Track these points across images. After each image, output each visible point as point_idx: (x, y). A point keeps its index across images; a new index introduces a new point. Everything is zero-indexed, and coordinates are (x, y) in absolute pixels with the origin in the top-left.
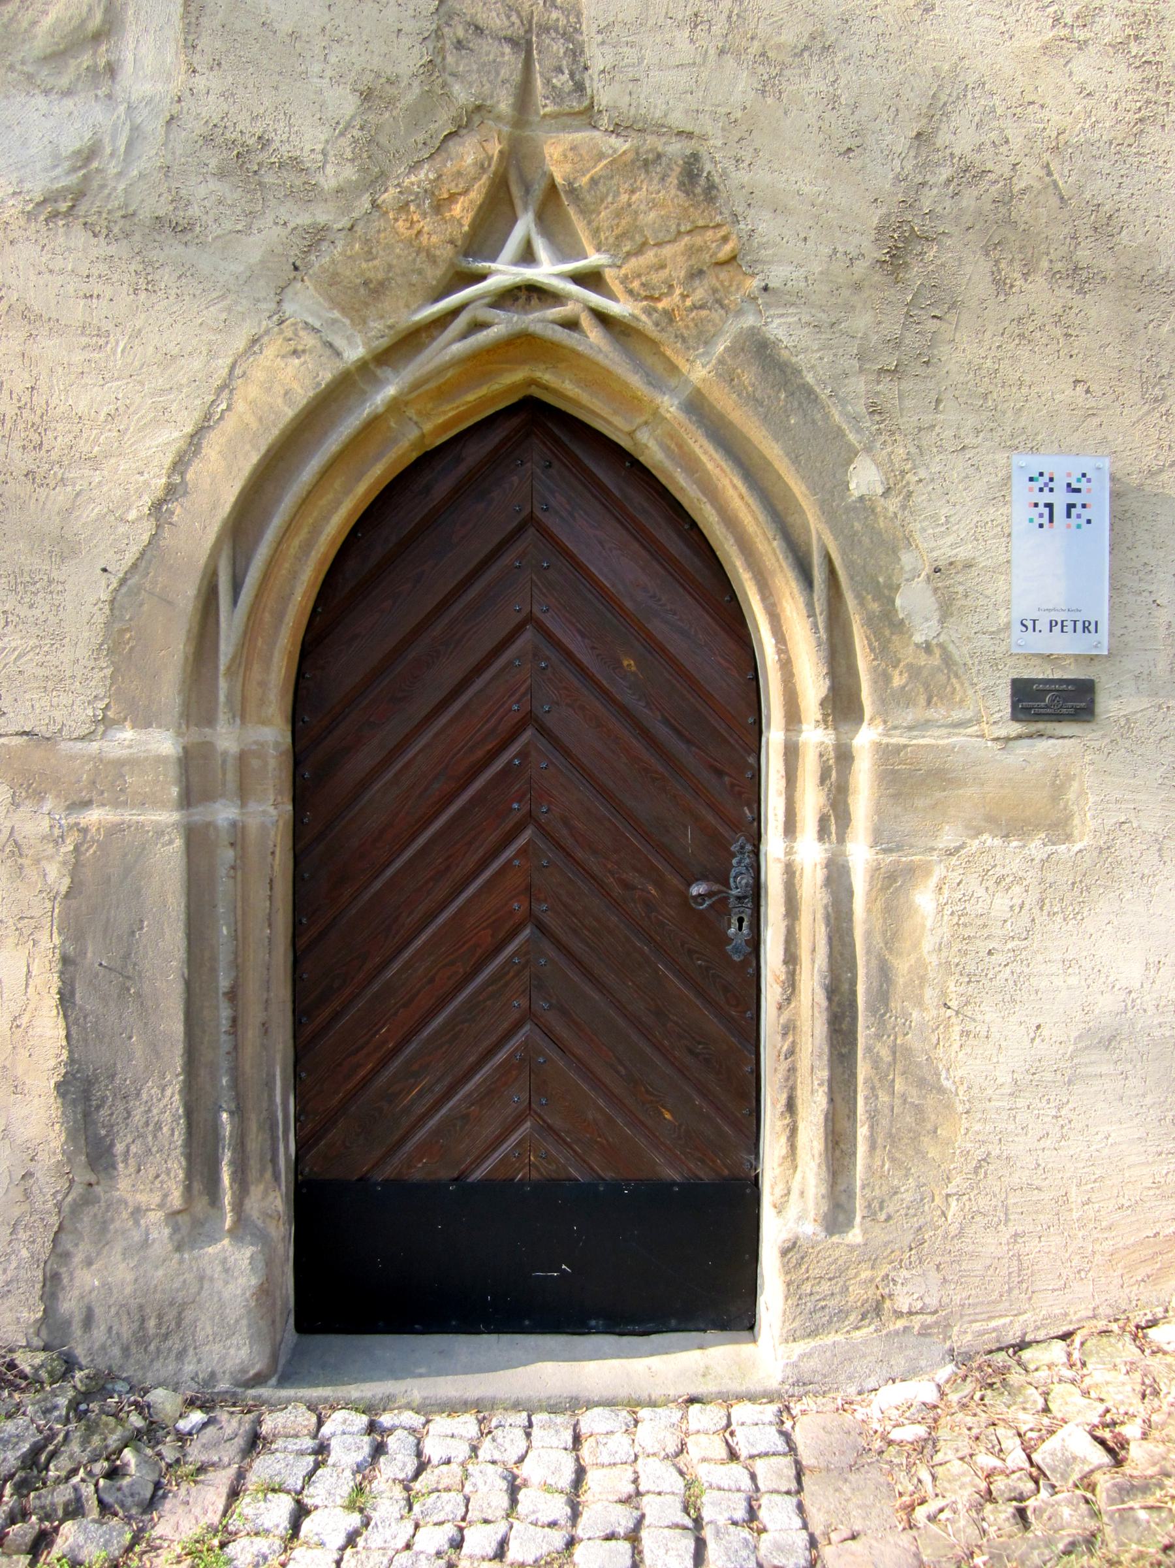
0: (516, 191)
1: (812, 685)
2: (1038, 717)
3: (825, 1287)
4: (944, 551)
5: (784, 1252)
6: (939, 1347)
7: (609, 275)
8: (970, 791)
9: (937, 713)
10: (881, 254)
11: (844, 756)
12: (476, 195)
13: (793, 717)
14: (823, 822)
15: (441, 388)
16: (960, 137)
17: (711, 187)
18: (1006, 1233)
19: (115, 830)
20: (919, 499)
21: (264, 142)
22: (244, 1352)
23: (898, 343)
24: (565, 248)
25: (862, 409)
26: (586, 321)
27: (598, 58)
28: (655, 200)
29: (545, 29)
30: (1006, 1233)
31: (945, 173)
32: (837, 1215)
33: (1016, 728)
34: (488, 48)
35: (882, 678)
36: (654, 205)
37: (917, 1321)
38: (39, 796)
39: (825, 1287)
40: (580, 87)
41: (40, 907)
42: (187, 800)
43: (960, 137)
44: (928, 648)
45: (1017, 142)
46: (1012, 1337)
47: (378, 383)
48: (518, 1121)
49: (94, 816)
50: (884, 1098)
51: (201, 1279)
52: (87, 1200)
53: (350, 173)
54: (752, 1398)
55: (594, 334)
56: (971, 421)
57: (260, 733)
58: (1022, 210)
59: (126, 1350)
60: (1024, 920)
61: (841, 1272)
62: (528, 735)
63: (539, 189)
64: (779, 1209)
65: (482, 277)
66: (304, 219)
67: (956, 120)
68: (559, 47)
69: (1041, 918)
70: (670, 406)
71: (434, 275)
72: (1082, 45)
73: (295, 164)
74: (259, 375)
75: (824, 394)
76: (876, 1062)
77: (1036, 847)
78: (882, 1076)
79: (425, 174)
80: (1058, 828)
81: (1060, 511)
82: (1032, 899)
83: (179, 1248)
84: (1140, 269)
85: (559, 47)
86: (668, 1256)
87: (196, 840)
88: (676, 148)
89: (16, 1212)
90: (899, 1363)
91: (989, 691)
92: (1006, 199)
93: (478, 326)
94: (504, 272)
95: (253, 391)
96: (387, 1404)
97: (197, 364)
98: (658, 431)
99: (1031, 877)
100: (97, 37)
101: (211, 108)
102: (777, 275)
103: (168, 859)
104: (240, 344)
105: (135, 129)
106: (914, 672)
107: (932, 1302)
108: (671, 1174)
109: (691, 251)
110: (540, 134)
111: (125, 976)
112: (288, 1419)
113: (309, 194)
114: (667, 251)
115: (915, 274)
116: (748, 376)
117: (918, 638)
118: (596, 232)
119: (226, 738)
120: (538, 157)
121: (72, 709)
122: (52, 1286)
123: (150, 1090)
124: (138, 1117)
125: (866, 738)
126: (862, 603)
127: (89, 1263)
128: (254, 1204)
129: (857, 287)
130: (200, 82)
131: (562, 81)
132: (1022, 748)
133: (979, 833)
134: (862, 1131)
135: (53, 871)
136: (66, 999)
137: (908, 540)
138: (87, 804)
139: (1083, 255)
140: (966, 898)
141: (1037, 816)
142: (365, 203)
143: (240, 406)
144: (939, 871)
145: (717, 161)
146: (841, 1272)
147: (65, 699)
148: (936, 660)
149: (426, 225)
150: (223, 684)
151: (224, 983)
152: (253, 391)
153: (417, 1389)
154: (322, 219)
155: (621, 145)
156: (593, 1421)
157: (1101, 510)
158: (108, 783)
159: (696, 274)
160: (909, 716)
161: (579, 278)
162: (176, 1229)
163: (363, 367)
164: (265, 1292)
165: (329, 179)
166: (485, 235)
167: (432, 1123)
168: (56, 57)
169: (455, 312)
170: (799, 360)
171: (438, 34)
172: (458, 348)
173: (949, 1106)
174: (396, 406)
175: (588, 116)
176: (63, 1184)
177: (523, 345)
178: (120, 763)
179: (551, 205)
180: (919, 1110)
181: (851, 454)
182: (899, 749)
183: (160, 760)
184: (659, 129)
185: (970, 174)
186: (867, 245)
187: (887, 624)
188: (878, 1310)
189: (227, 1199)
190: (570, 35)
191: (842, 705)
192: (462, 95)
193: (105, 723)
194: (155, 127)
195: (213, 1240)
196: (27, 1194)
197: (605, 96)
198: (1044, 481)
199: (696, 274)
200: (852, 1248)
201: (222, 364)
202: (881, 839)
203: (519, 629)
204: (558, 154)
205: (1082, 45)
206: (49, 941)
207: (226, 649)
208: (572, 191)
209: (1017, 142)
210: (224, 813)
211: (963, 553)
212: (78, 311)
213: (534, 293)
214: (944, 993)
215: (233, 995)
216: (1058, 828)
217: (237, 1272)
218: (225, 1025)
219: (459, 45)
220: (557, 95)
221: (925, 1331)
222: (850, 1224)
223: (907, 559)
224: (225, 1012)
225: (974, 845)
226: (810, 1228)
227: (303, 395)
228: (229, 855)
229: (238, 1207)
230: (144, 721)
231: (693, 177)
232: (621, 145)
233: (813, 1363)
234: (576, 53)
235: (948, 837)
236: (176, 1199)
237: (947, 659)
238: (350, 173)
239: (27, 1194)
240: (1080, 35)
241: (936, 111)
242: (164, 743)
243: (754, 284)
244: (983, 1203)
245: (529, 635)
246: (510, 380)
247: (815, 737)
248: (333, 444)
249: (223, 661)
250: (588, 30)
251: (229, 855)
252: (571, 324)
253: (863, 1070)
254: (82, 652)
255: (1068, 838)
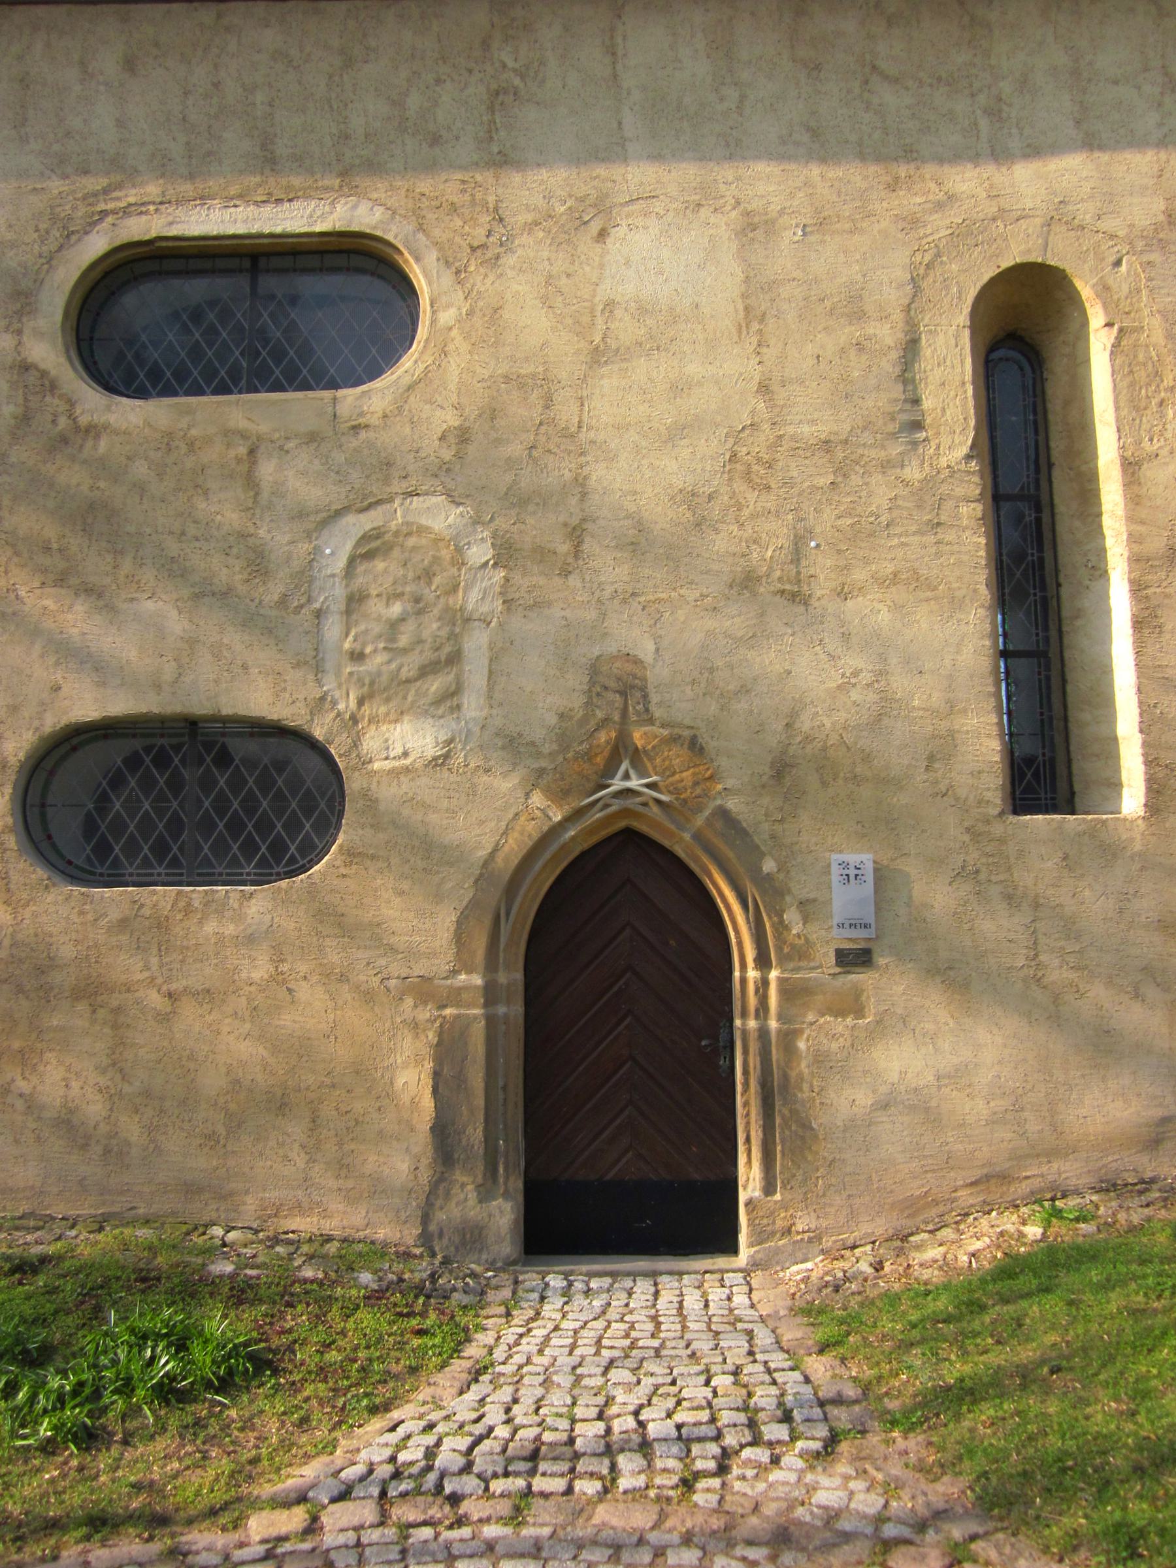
0: (622, 750)
1: (750, 954)
2: (847, 964)
3: (765, 1221)
4: (804, 894)
5: (746, 1205)
6: (817, 1249)
7: (661, 784)
8: (820, 997)
9: (803, 964)
10: (773, 773)
11: (765, 982)
12: (606, 753)
13: (743, 966)
14: (757, 1011)
15: (590, 831)
16: (805, 724)
17: (702, 749)
18: (845, 1194)
19: (458, 1017)
20: (793, 874)
21: (520, 735)
22: (508, 1250)
23: (781, 809)
24: (642, 774)
25: (767, 837)
26: (651, 803)
27: (654, 698)
28: (677, 756)
29: (633, 687)
30: (845, 1194)
31: (799, 739)
32: (769, 1188)
33: (838, 970)
34: (610, 696)
35: (779, 949)
36: (678, 756)
37: (806, 1236)
38: (425, 1003)
39: (765, 1221)
40: (647, 710)
41: (426, 1051)
42: (486, 1005)
43: (805, 724)
44: (799, 936)
45: (828, 725)
46: (849, 1243)
47: (566, 830)
48: (626, 1151)
49: (448, 1012)
50: (787, 1132)
51: (490, 1216)
52: (441, 1180)
53: (555, 747)
54: (734, 1271)
55: (655, 809)
56: (814, 840)
57: (512, 976)
58: (831, 752)
59: (457, 1249)
60: (845, 1053)
61: (772, 1213)
62: (628, 975)
63: (631, 749)
64: (745, 1188)
65: (608, 786)
66: (536, 765)
67: (802, 718)
68: (638, 694)
69: (853, 1052)
70: (687, 836)
71: (590, 786)
72: (854, 685)
73: (533, 744)
74: (518, 828)
75: (751, 831)
76: (783, 1117)
77: (849, 1021)
78: (786, 1124)
79: (585, 746)
80: (859, 1013)
81: (852, 877)
82: (848, 1044)
83: (480, 1202)
84: (883, 775)
85: (638, 694)
86: (696, 1221)
87: (491, 1020)
88: (686, 733)
89: (411, 1185)
90: (800, 1255)
91: (825, 954)
92: (824, 749)
93: (607, 806)
94: (617, 784)
95: (516, 835)
96: (571, 1273)
97: (493, 824)
98: (682, 845)
99: (847, 1033)
100: (453, 694)
101: (498, 722)
102: (730, 783)
103: (478, 1032)
104: (511, 816)
105: (469, 731)
106: (793, 946)
107: (813, 1226)
108: (696, 1176)
109: (694, 774)
110: (632, 728)
111: (460, 1080)
112: (530, 1278)
113: (539, 755)
114: (684, 774)
115: (787, 781)
116: (719, 825)
117: (794, 932)
118: (654, 768)
119: (502, 978)
120: (631, 736)
121: (443, 964)
122: (425, 1219)
123: (470, 1130)
124: (464, 1142)
125: (774, 974)
126: (770, 918)
127: (441, 1208)
128: (511, 1184)
129: (764, 786)
130: (494, 712)
131: (640, 707)
132: (841, 979)
133: (823, 1015)
134: (779, 1148)
135: (431, 1035)
136: (435, 1091)
137: (789, 891)
138: (445, 1006)
139: (858, 770)
140: (820, 1043)
141: (852, 1006)
142: (560, 758)
143: (510, 841)
144: (807, 1032)
145: (705, 739)
146: (772, 1213)
147: (437, 962)
148: (802, 941)
149: (586, 766)
150: (501, 955)
151: (501, 1083)
152: (516, 835)
153: (584, 1268)
154: (544, 765)
155: (665, 732)
156: (661, 1279)
157: (870, 877)
158: (455, 996)
159: (696, 784)
160: (791, 965)
161: (648, 786)
162: (479, 1193)
163: (560, 823)
164: (516, 1221)
165: (546, 749)
166: (609, 770)
167: (587, 1153)
168: (437, 703)
169: (597, 801)
170: (740, 817)
171: (590, 690)
172: (598, 815)
173: (816, 1137)
174: (573, 838)
175: (651, 721)
176: (431, 1172)
177: (626, 812)
178: (460, 988)
179: (638, 759)
180: (803, 1138)
181: (763, 855)
182: (787, 979)
183: (476, 987)
184: (680, 725)
185: (809, 739)
186: (767, 770)
187: (781, 927)
188: (789, 1231)
189: (501, 1180)
190: (643, 689)
191: (763, 962)
192: (600, 714)
193: (454, 972)
194: (477, 730)
195: (495, 1199)
196: (416, 1177)
197: (658, 713)
198: (845, 865)
199: (696, 784)
200: (776, 1202)
201: (503, 824)
202: (780, 1017)
203: (623, 928)
204: (638, 736)
205: (854, 685)
206: (429, 1065)
207: (503, 940)
208: (645, 751)
209: (828, 725)
210: (501, 1010)
211: (812, 896)
212: (445, 803)
213: (629, 791)
214: (812, 1086)
215: (505, 1088)
216: (859, 1013)
217: (503, 1215)
218: (501, 1101)
219: (598, 694)
220: (638, 713)
221: (810, 1240)
222: (775, 1192)
223: (788, 899)
224: (501, 1096)
225: (822, 1020)
226: (757, 1194)
227: (536, 836)
228: (503, 1027)
229: (505, 1183)
230: (470, 972)
231: (695, 747)
232: (665, 732)
233: (760, 1256)
234: (645, 696)
235: (810, 1017)
236: (480, 1180)
237: (807, 940)
238: (555, 747)
239: (416, 1177)
240: (853, 681)
241: (793, 715)
242: (478, 980)
243: (720, 787)
244: (833, 1180)
245: (627, 932)
246: (622, 824)
247: (752, 974)
248: (547, 856)
249: (502, 947)
250: (651, 689)
251: (503, 1027)
252: (645, 804)
253: (778, 1121)
254: (444, 942)
255: (863, 1017)
